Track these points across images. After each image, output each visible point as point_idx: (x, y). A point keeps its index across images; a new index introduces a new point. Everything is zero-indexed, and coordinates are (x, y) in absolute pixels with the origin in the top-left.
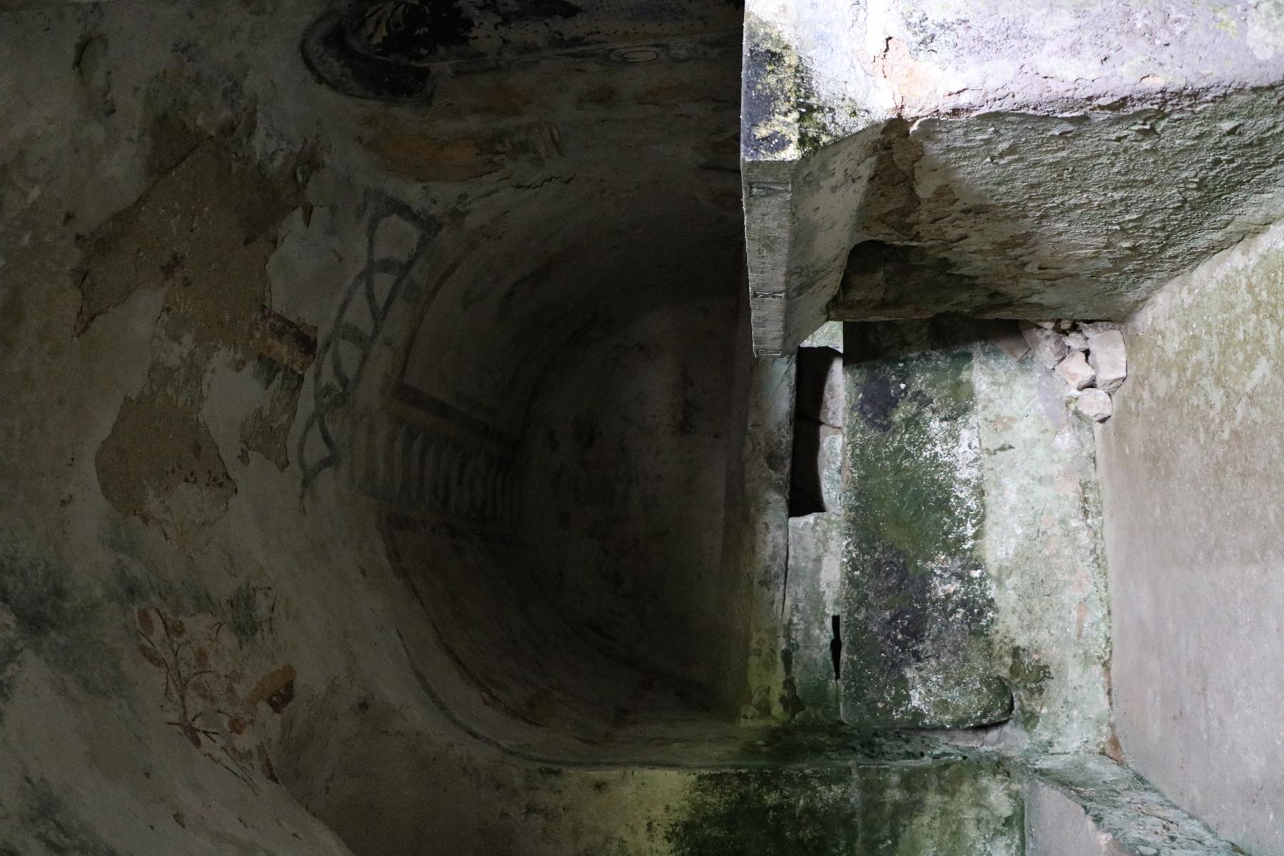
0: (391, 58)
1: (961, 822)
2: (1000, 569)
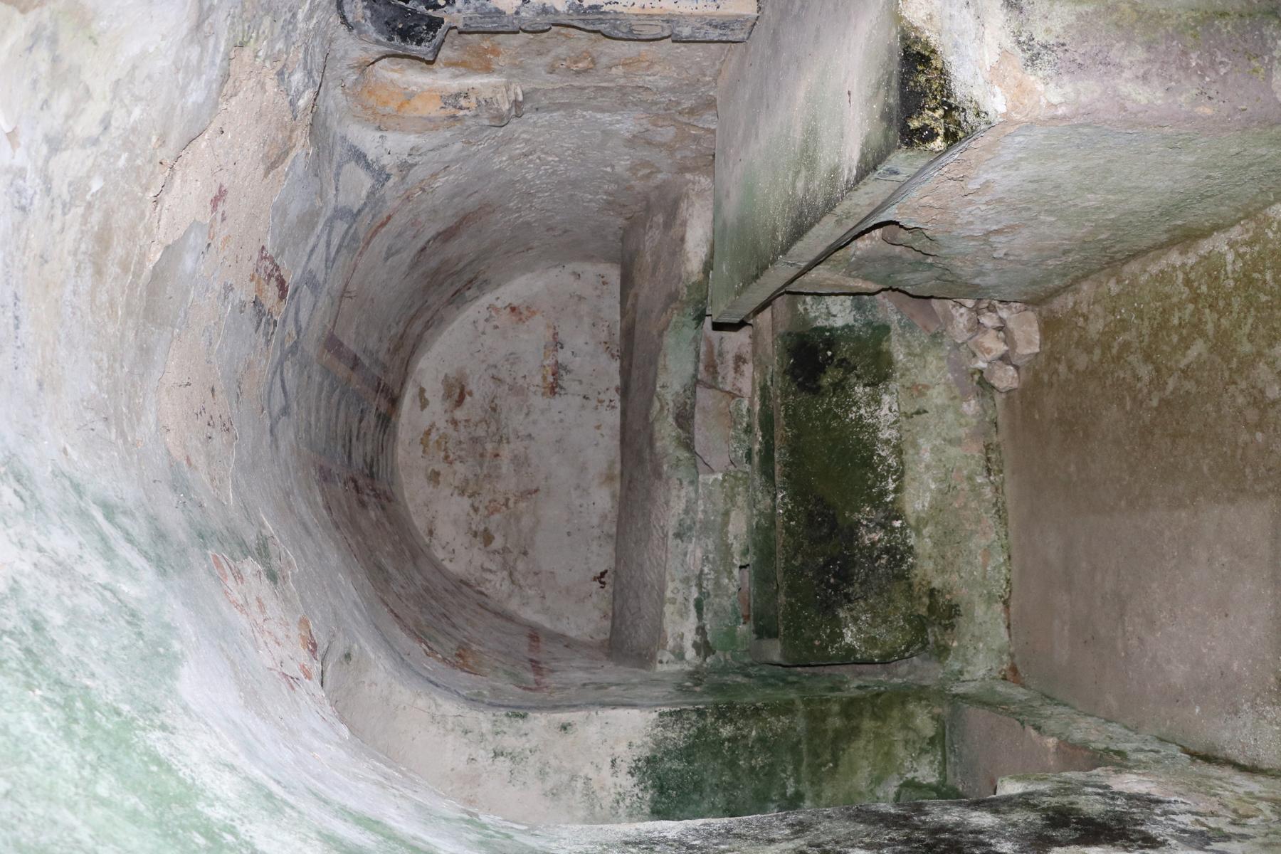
1: (892, 744)
2: (918, 520)
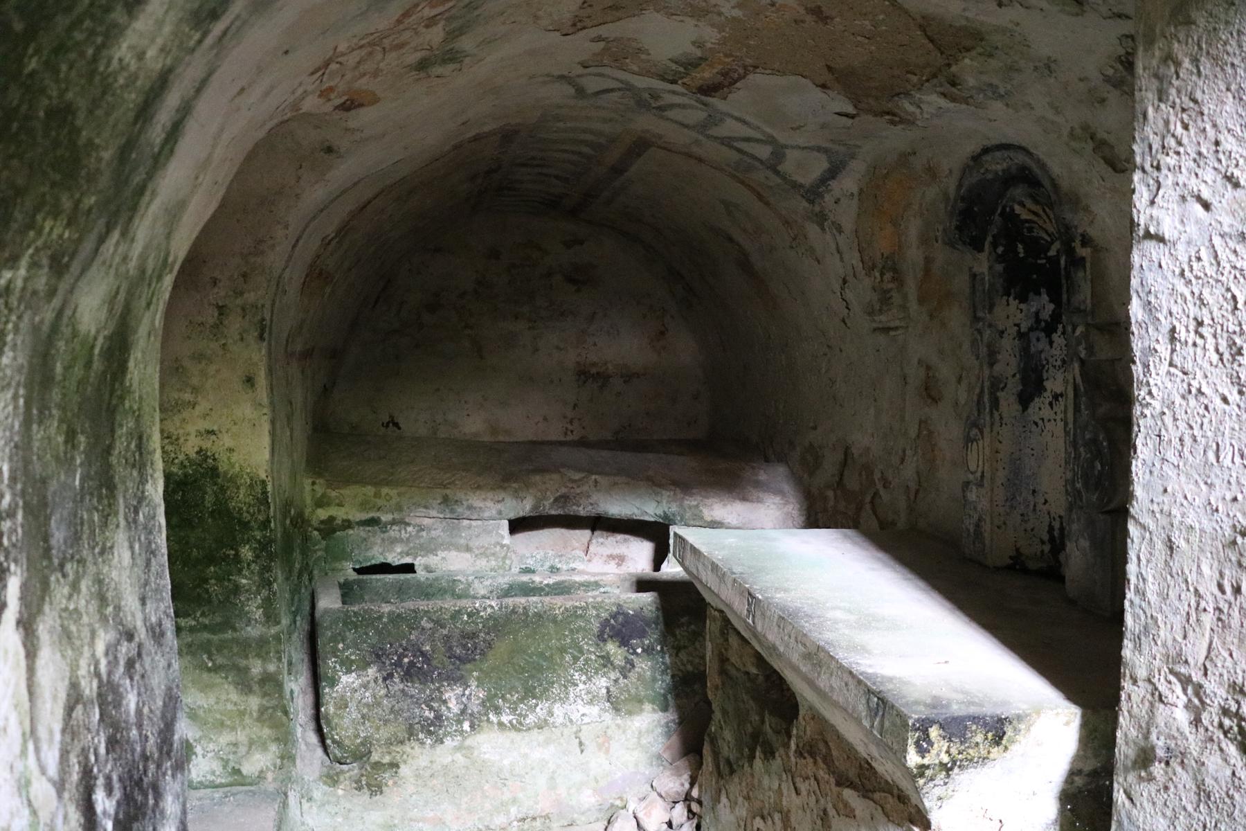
0: (997, 217)
1: (233, 729)
2: (470, 748)
